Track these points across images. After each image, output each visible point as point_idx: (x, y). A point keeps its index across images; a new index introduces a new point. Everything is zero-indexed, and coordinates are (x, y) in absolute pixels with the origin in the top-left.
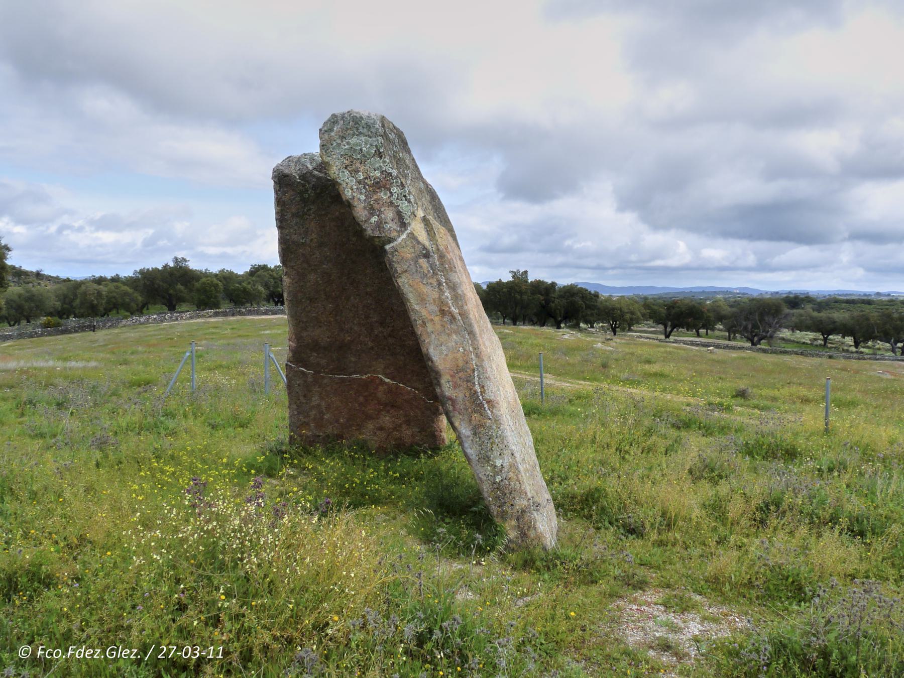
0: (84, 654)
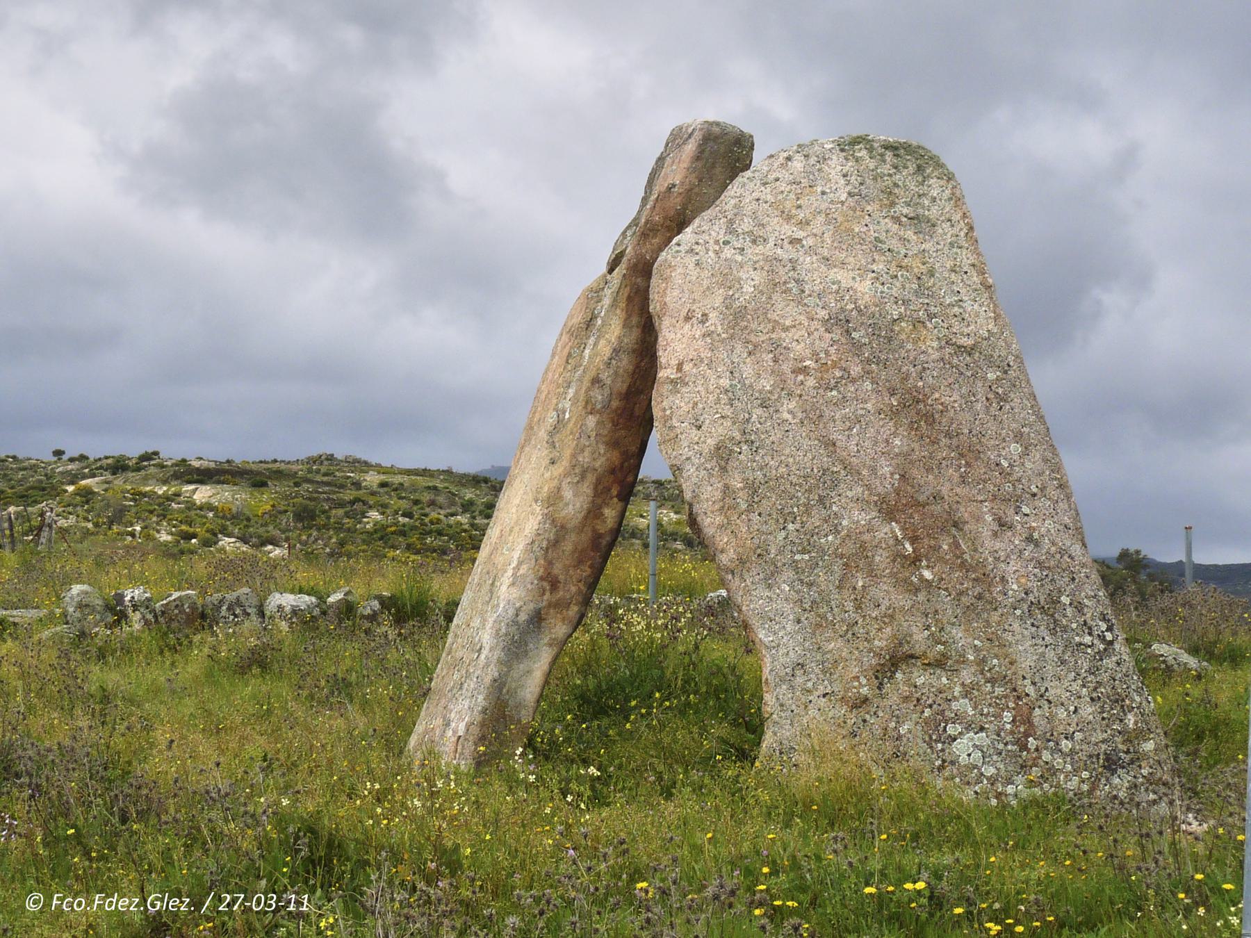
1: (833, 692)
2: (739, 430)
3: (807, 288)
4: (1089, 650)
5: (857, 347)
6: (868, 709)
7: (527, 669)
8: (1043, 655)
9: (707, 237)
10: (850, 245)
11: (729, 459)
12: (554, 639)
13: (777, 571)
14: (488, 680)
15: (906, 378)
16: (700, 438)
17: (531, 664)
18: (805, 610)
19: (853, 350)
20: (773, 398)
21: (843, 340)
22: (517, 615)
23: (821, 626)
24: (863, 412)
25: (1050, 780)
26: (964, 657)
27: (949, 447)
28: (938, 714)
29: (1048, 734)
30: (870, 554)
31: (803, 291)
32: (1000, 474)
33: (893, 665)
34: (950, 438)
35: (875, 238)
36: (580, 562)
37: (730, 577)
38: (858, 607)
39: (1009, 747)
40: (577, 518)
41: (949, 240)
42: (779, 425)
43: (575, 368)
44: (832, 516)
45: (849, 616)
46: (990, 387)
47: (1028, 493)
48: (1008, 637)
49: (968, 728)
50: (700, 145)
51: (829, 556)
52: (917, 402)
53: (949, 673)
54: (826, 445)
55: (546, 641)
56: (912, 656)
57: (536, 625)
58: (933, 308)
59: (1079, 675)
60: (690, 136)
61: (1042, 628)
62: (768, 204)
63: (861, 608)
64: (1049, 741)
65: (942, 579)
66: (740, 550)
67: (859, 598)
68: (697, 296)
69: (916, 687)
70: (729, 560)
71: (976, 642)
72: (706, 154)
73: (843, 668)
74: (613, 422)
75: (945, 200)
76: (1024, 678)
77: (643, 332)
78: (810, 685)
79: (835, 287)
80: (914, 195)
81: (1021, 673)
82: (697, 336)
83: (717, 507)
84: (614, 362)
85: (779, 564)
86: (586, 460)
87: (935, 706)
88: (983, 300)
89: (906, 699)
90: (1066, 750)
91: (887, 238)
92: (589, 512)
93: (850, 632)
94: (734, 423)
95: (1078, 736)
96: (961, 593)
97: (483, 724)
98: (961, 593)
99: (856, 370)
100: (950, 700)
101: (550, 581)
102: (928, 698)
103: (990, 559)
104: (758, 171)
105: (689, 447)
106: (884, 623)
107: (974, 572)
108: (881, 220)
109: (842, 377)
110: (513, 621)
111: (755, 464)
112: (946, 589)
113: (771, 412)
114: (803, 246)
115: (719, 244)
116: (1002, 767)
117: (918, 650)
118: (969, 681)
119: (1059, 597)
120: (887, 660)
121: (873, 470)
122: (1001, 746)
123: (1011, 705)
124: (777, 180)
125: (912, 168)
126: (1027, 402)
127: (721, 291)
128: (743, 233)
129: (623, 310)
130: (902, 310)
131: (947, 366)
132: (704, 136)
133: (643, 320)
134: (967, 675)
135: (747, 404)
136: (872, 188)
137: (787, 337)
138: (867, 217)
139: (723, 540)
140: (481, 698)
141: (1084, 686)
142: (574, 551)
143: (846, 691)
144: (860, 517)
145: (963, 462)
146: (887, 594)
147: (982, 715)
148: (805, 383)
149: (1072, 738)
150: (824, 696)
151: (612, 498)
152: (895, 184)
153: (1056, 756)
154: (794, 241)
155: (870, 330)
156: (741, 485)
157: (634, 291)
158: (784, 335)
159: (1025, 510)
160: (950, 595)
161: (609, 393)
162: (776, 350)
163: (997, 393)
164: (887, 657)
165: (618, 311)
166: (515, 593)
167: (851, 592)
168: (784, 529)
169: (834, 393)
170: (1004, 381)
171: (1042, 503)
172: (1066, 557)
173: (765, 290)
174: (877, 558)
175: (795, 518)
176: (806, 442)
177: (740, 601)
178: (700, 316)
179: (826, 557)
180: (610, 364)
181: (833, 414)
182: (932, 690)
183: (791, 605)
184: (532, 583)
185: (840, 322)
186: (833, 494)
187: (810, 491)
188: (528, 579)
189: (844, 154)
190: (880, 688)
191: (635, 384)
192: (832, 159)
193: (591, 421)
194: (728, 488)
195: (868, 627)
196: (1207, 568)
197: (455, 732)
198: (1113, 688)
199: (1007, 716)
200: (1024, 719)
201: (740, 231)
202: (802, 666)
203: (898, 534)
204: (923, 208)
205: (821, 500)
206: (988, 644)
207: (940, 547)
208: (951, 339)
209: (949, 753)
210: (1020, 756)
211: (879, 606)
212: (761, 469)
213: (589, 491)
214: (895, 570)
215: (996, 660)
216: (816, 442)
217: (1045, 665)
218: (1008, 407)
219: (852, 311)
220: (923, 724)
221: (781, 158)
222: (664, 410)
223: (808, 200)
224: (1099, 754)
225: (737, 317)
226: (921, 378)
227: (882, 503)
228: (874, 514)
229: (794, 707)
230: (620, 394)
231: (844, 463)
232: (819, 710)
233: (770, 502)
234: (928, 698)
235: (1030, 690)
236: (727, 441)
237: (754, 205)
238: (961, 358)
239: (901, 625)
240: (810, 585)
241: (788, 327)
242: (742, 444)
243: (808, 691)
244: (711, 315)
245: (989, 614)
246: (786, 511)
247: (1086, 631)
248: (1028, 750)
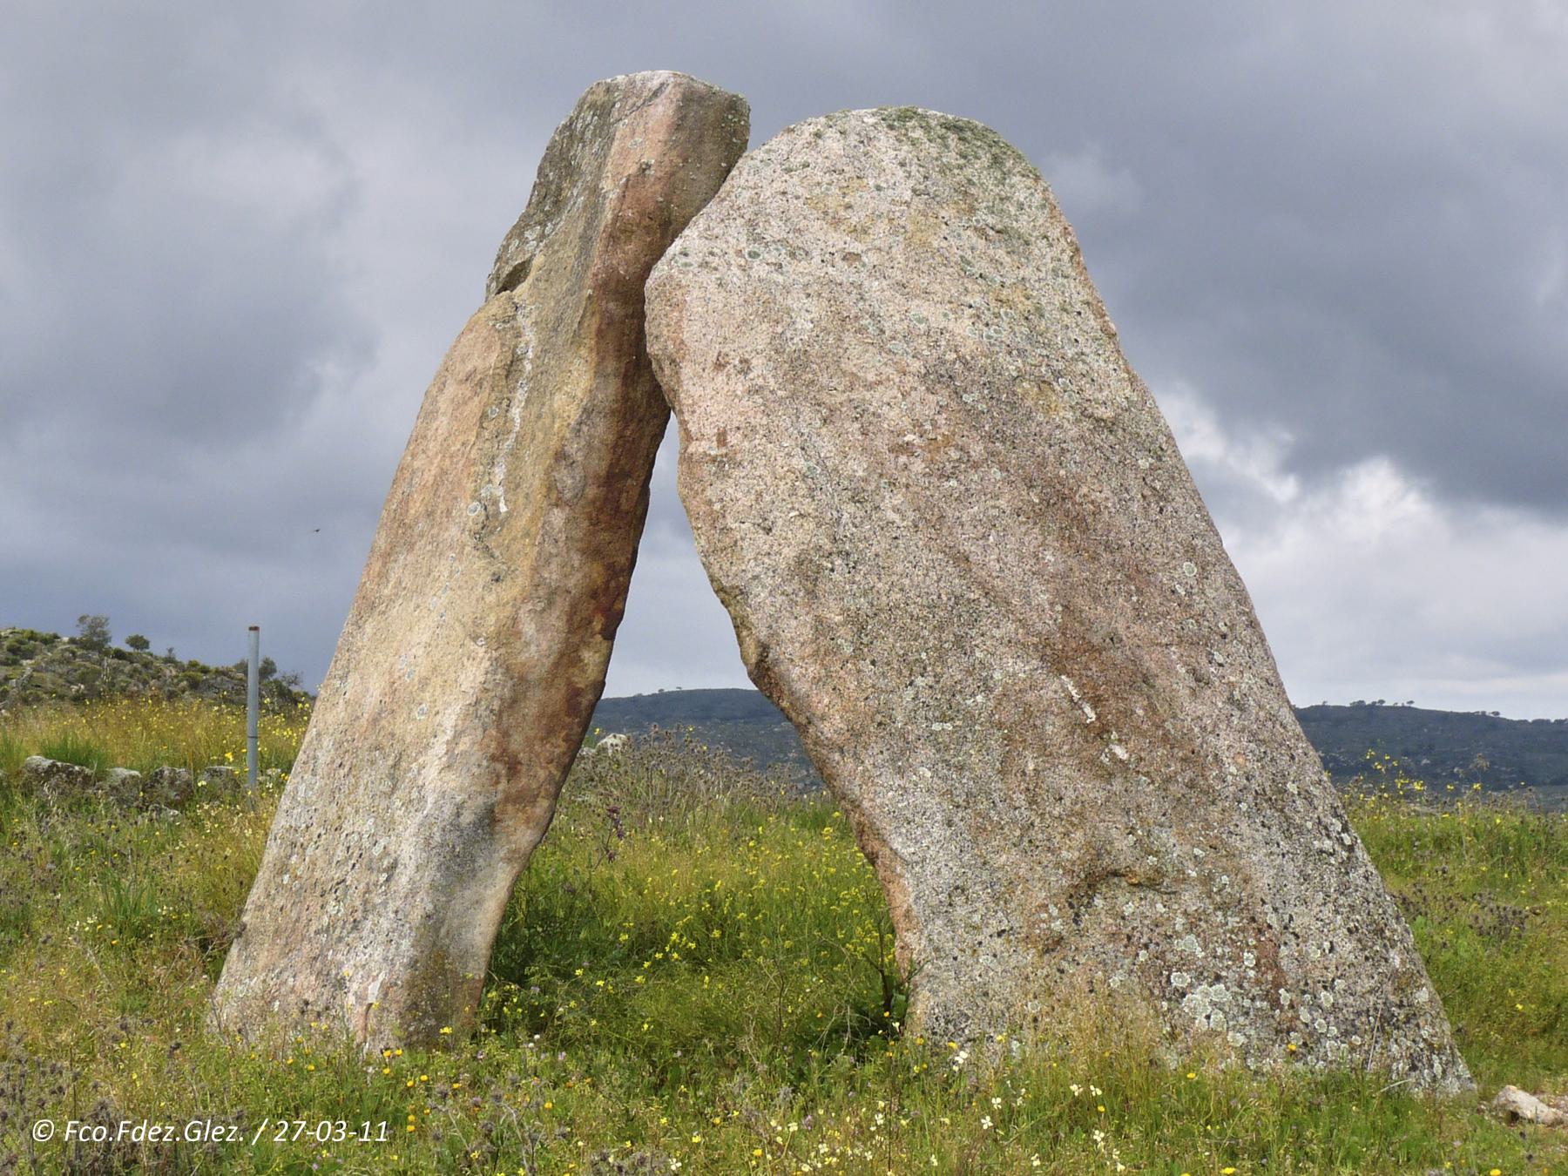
0: (147, 1133)
1: (1012, 929)
2: (828, 536)
3: (887, 325)
4: (1332, 861)
5: (972, 415)
6: (1065, 952)
7: (475, 898)
8: (1281, 868)
9: (724, 246)
10: (930, 265)
11: (817, 579)
12: (514, 851)
13: (908, 748)
14: (416, 916)
15: (1042, 465)
16: (771, 546)
18: (958, 807)
19: (969, 420)
20: (869, 488)
21: (953, 405)
22: (458, 815)
23: (985, 830)
24: (995, 512)
25: (1316, 1050)
26: (1184, 873)
27: (1113, 565)
28: (1157, 958)
29: (1302, 983)
30: (1038, 722)
31: (882, 332)
32: (1179, 605)
33: (1089, 886)
34: (1111, 552)
35: (962, 257)
36: (550, 732)
37: (837, 756)
38: (1032, 802)
39: (1258, 1004)
40: (543, 665)
41: (1051, 266)
42: (882, 529)
43: (498, 436)
44: (978, 666)
45: (1021, 814)
46: (1144, 479)
47: (1217, 634)
48: (1235, 841)
49: (1200, 977)
50: (680, 108)
51: (981, 724)
52: (1063, 499)
53: (1165, 897)
54: (956, 560)
56: (1115, 874)
57: (487, 829)
58: (1055, 363)
59: (1329, 896)
60: (655, 94)
61: (1274, 829)
62: (802, 201)
63: (1036, 802)
64: (1304, 992)
65: (1141, 759)
66: (850, 716)
67: (1031, 787)
68: (728, 332)
69: (1123, 918)
70: (835, 731)
71: (1197, 851)
72: (689, 122)
73: (1023, 893)
74: (590, 519)
75: (1036, 207)
76: (1264, 903)
77: (624, 384)
78: (976, 918)
79: (923, 327)
80: (995, 199)
81: (1259, 895)
82: (739, 393)
83: (808, 650)
84: (585, 428)
85: (911, 738)
86: (554, 577)
87: (1152, 946)
88: (1107, 354)
89: (1113, 936)
90: (1327, 1005)
91: (974, 258)
92: (562, 655)
93: (1026, 839)
94: (819, 525)
95: (1340, 984)
96: (1169, 780)
97: (411, 985)
98: (1169, 780)
99: (977, 450)
100: (1171, 937)
102: (1142, 934)
103: (1197, 730)
104: (774, 151)
105: (755, 559)
106: (1072, 823)
107: (1181, 748)
108: (961, 232)
109: (959, 460)
110: (451, 824)
111: (855, 586)
112: (1147, 774)
113: (869, 509)
114: (864, 265)
115: (743, 257)
116: (1252, 1032)
117: (1121, 865)
118: (1195, 908)
119: (1285, 784)
120: (1082, 880)
121: (1026, 597)
122: (1247, 1003)
123: (1252, 942)
124: (806, 165)
125: (986, 159)
126: (1191, 502)
127: (764, 326)
128: (774, 242)
129: (591, 350)
130: (1020, 363)
131: (1090, 448)
132: (684, 95)
133: (623, 365)
134: (1190, 899)
135: (833, 498)
136: (942, 186)
137: (875, 398)
138: (944, 226)
139: (822, 701)
140: (406, 944)
141: (1337, 912)
142: (540, 717)
143: (1033, 925)
144: (1017, 667)
145: (1133, 588)
146: (1069, 781)
147: (1215, 957)
148: (910, 467)
149: (1333, 989)
150: (1000, 934)
151: (593, 635)
152: (969, 181)
153: (1315, 1014)
154: (850, 257)
155: (986, 392)
156: (840, 618)
157: (606, 321)
158: (868, 396)
159: (1219, 658)
160: (1153, 782)
161: (582, 474)
162: (862, 416)
163: (1155, 489)
164: (1083, 876)
165: (583, 352)
166: (453, 781)
167: (1020, 778)
168: (911, 684)
169: (953, 483)
170: (1160, 471)
171: (1235, 647)
172: (1278, 726)
173: (830, 327)
174: (1049, 729)
175: (925, 669)
176: (925, 555)
177: (857, 793)
178: (737, 362)
179: (977, 727)
180: (579, 431)
181: (957, 513)
182: (1146, 922)
183: (937, 799)
184: (479, 766)
185: (938, 377)
186: (973, 633)
187: (940, 628)
188: (473, 759)
189: (894, 133)
190: (1077, 919)
191: (619, 460)
192: (879, 140)
193: (558, 517)
194: (821, 623)
195: (1049, 830)
196: (636, 701)
197: (360, 998)
198: (1369, 914)
199: (1249, 959)
200: (1268, 962)
201: (768, 238)
202: (963, 891)
203: (1073, 693)
204: (1009, 216)
205: (959, 641)
206: (1212, 853)
207: (1133, 712)
208: (1086, 409)
209: (1180, 1016)
210: (1273, 1017)
211: (1061, 799)
212: (865, 594)
213: (561, 624)
214: (1076, 746)
215: (1224, 877)
216: (941, 556)
217: (1285, 882)
218: (1170, 509)
219: (954, 363)
220: (1139, 974)
221: (807, 134)
222: (710, 503)
223: (860, 197)
224: (1368, 1010)
225: (796, 366)
226: (1061, 464)
227: (1045, 647)
228: (1035, 663)
229: (956, 952)
230: (597, 476)
231: (984, 588)
232: (995, 956)
233: (887, 644)
234: (1142, 934)
235: (1272, 919)
236: (812, 552)
237: (780, 202)
238: (1104, 437)
239: (1096, 828)
240: (961, 768)
241: (871, 383)
242: (834, 557)
243: (974, 928)
244: (754, 362)
245: (1206, 809)
246: (911, 658)
247: (1324, 832)
248: (1281, 1007)
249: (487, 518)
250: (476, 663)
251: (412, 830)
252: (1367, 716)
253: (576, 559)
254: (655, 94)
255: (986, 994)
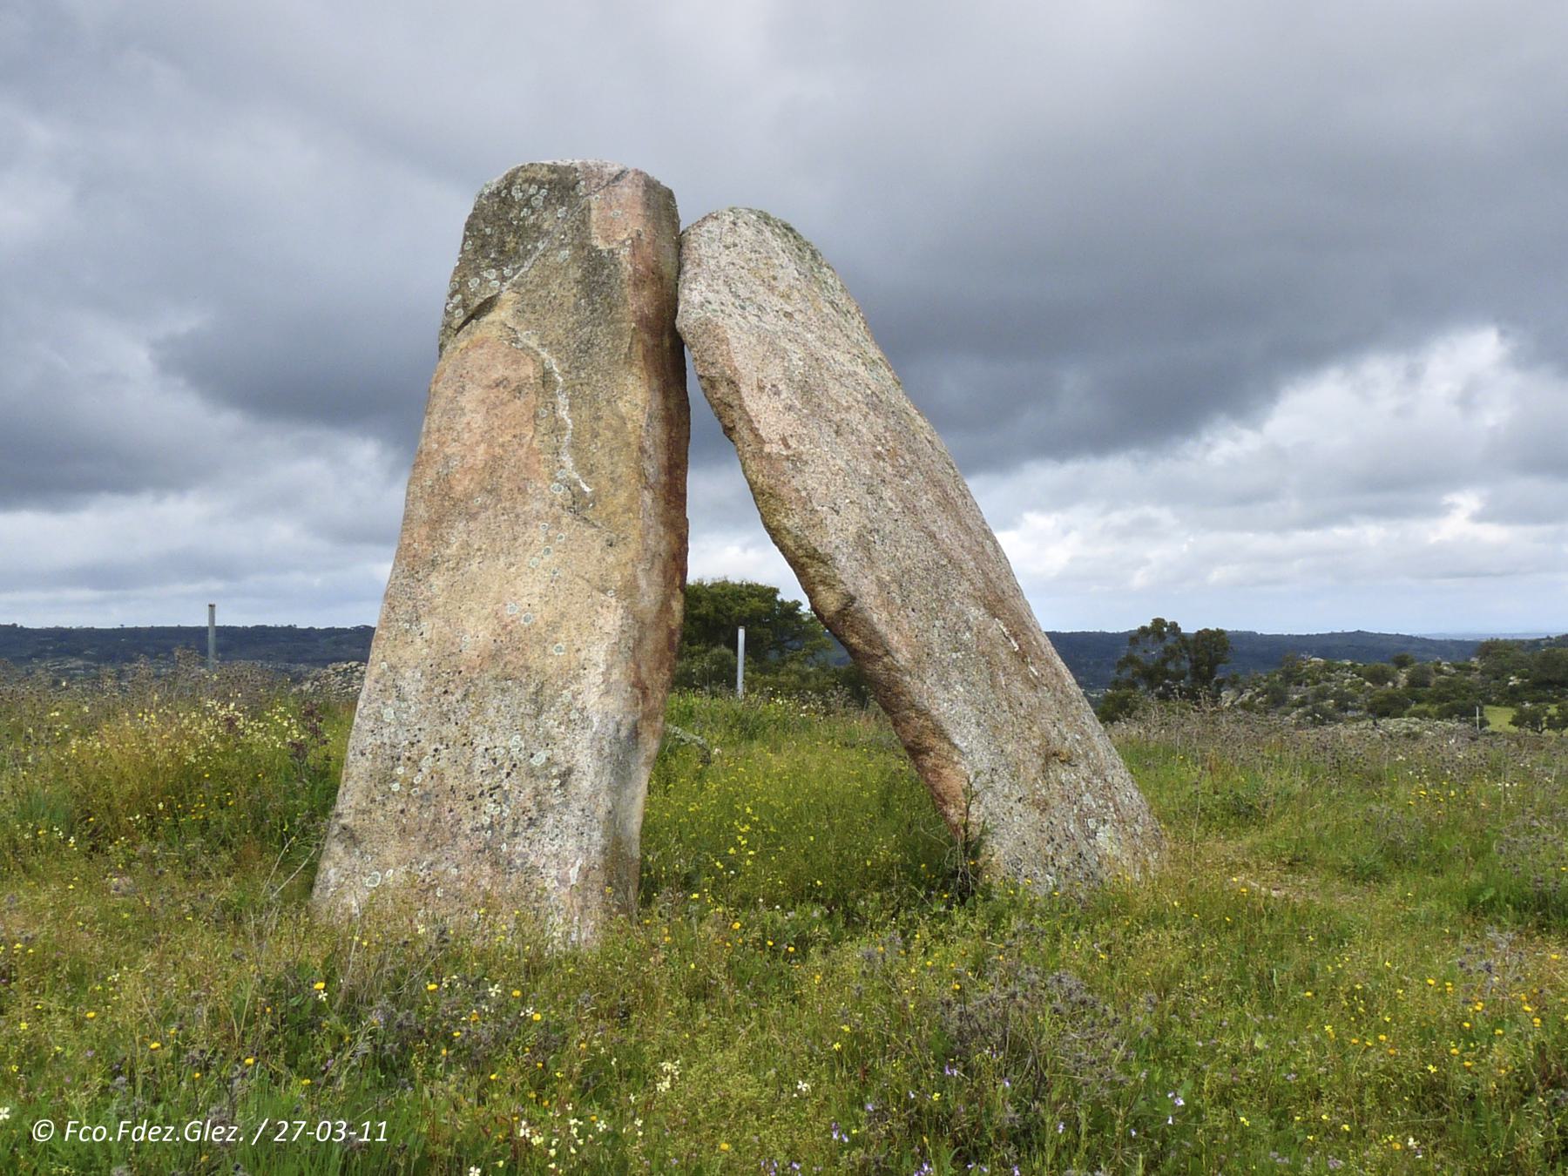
14: (601, 812)
17: (634, 788)
22: (618, 731)
55: (642, 760)
101: (641, 688)
129: (641, 369)
139: (895, 639)
140: (597, 835)
196: (246, 632)
221: (727, 223)
222: (797, 490)
229: (1002, 816)
249: (574, 496)
250: (611, 609)
251: (586, 743)
252: (1054, 633)
253: (661, 530)
254: (617, 178)
255: (1024, 843)
